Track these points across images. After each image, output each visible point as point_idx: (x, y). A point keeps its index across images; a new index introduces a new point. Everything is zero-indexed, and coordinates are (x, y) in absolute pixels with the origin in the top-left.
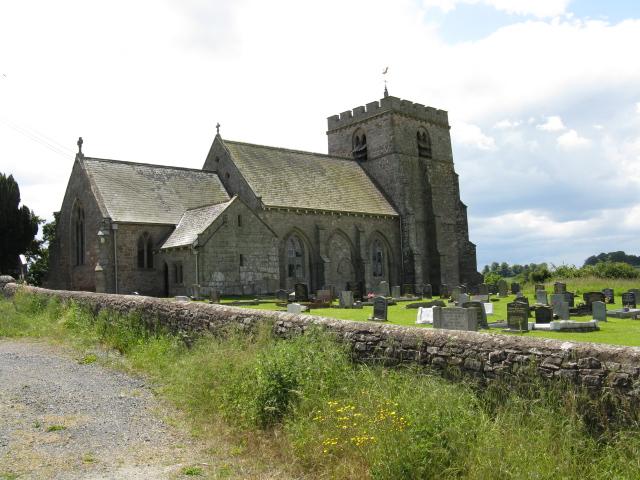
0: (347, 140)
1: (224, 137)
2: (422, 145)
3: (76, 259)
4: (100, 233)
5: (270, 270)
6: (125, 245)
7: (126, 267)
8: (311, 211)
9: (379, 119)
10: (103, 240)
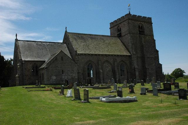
0: (115, 30)
1: (68, 31)
2: (140, 30)
4: (18, 64)
5: (74, 75)
8: (96, 55)
9: (124, 22)
10: (19, 67)
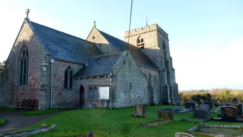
3: (19, 78)
6: (58, 73)
7: (57, 87)
